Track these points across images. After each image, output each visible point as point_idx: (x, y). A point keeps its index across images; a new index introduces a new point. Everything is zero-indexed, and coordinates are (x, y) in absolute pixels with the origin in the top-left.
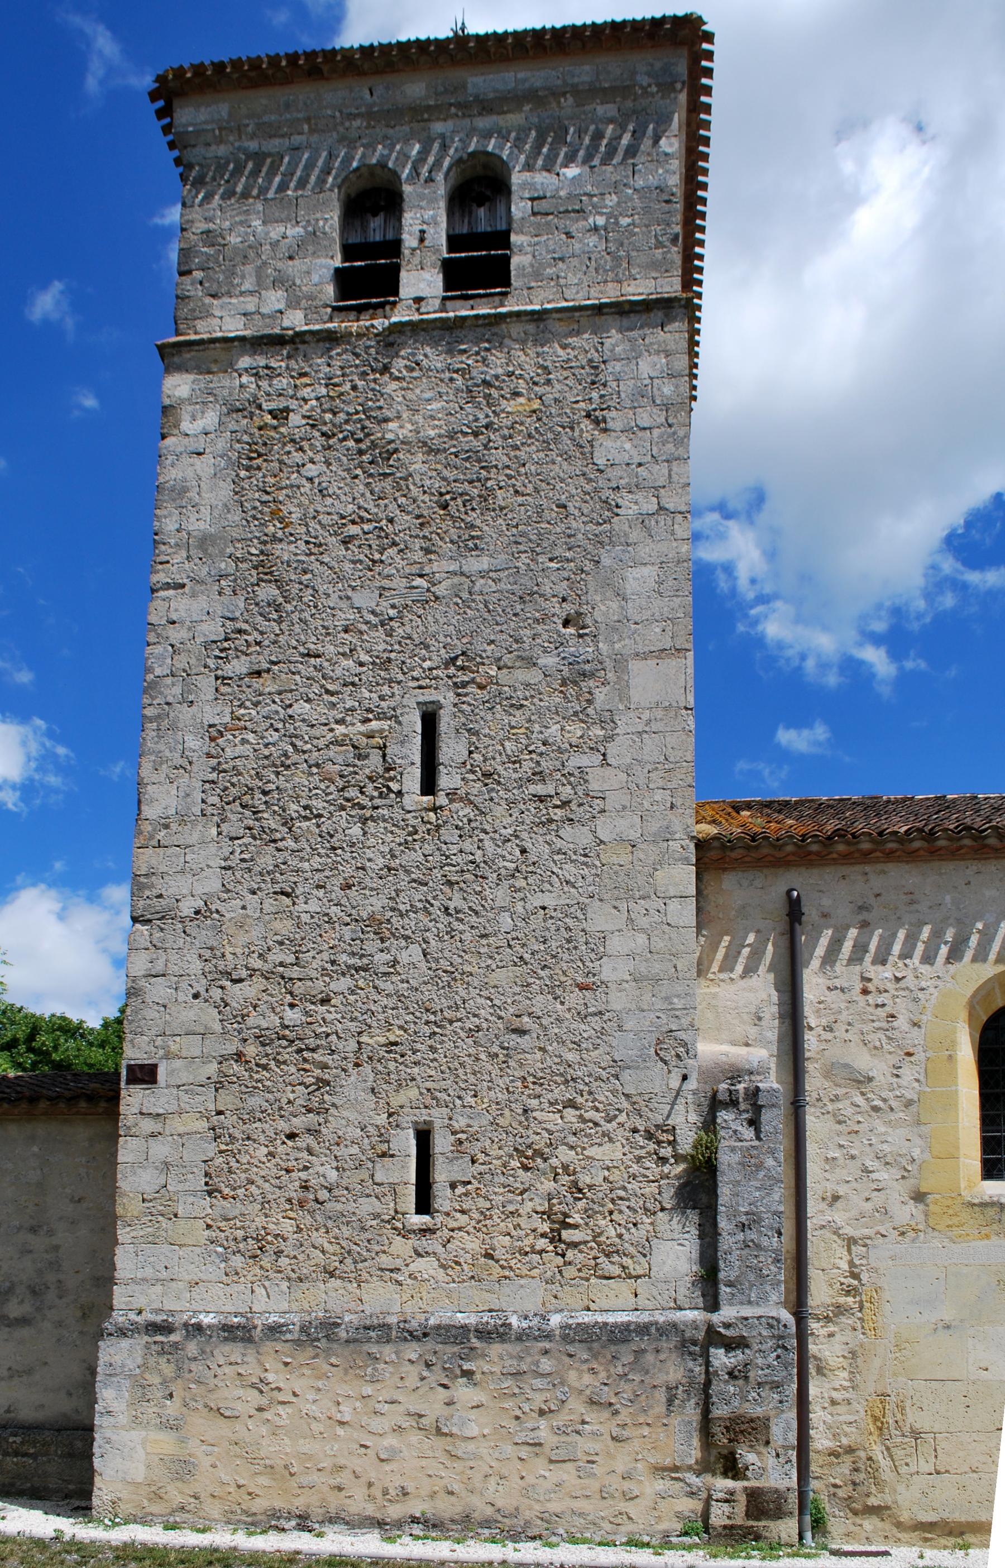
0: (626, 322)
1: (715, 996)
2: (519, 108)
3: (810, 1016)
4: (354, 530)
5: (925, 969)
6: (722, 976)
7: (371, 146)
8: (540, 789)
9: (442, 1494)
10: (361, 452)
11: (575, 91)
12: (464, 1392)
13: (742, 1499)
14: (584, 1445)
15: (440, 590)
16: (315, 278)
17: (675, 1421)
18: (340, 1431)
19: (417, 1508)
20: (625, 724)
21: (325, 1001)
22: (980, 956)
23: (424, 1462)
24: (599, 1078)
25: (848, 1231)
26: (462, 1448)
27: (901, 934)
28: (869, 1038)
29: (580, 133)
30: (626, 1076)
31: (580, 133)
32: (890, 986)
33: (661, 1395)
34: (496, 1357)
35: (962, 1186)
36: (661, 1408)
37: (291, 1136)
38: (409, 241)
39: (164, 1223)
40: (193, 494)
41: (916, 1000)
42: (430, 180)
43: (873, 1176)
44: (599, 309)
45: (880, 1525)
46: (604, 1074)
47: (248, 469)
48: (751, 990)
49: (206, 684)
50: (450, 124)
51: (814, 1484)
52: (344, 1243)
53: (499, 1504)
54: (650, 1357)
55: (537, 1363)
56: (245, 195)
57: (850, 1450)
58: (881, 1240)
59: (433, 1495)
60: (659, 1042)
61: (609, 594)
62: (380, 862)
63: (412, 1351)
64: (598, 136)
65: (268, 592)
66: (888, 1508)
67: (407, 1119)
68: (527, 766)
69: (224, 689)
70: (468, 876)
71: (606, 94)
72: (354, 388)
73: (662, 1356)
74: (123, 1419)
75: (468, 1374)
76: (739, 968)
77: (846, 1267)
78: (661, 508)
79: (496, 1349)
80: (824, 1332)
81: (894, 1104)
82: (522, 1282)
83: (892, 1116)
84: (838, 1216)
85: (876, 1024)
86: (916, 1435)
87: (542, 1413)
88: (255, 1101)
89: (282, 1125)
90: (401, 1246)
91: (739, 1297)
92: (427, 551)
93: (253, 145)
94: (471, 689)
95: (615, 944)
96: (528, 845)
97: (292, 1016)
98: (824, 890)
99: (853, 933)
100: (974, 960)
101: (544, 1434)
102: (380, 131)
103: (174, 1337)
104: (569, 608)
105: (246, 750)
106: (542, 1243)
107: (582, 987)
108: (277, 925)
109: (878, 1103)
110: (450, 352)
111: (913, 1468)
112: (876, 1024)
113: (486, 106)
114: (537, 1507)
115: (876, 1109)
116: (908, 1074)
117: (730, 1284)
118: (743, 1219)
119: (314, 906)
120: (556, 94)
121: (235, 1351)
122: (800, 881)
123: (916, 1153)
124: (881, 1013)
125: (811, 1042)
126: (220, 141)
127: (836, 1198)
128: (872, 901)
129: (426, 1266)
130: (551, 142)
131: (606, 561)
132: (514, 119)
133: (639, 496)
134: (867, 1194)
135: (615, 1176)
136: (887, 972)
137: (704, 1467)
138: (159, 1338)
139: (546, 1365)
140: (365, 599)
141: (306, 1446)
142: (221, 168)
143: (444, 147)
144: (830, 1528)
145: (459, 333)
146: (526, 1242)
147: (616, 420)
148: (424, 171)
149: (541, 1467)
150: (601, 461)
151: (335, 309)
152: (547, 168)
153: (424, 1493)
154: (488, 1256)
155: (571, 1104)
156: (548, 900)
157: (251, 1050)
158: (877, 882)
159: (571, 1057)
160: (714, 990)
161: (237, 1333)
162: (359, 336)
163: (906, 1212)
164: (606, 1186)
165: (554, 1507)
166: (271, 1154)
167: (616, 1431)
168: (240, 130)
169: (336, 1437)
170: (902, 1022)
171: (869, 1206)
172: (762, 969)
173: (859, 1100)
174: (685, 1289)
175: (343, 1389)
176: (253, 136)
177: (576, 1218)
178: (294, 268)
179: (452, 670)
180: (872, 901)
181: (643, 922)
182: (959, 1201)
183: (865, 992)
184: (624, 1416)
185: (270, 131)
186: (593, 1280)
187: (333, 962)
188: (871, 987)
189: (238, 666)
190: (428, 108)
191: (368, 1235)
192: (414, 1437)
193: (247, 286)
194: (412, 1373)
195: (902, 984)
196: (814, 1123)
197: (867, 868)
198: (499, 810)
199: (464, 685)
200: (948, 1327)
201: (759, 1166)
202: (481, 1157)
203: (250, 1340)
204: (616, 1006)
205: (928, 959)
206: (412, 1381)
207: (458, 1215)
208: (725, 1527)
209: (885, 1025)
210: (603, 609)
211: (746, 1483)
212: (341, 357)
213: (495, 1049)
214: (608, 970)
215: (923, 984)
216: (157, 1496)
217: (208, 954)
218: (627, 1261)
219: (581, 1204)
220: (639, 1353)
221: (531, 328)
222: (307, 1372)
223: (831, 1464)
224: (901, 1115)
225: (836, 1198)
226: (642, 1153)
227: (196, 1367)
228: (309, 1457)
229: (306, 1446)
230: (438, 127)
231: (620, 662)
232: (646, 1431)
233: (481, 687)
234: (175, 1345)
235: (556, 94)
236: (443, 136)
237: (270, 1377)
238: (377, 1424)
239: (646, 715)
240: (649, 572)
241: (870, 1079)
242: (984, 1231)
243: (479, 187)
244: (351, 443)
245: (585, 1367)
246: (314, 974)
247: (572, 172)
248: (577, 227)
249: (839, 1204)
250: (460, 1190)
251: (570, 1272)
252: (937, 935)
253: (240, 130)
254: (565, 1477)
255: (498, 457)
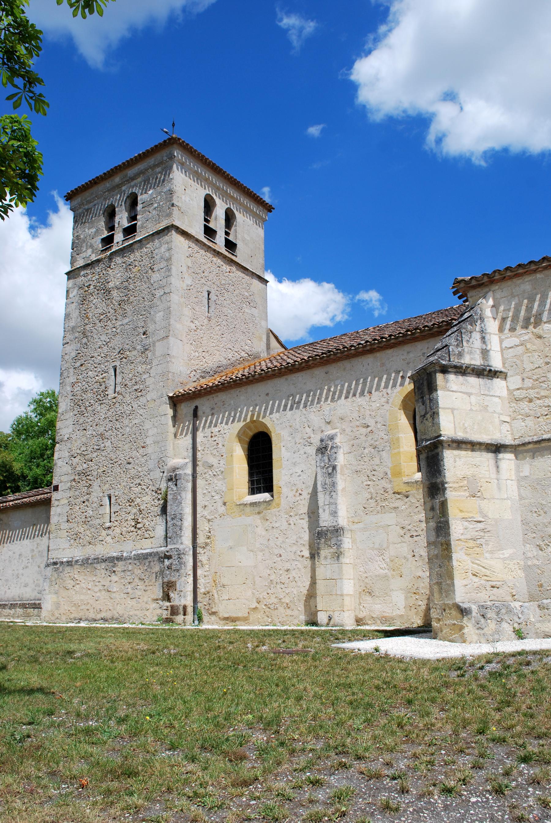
0: (159, 236)
1: (178, 443)
2: (140, 176)
3: (199, 447)
4: (102, 317)
5: (226, 427)
6: (181, 437)
7: (109, 199)
8: (136, 387)
9: (108, 610)
10: (104, 293)
11: (150, 167)
12: (114, 578)
13: (170, 608)
14: (138, 593)
15: (118, 331)
16: (97, 243)
17: (157, 584)
18: (89, 592)
19: (103, 615)
20: (155, 362)
21: (91, 461)
22: (239, 421)
23: (105, 601)
24: (145, 476)
25: (208, 517)
26: (113, 595)
27: (221, 416)
28: (212, 452)
29: (153, 179)
30: (151, 473)
31: (153, 179)
32: (217, 434)
33: (154, 575)
34: (121, 565)
35: (235, 499)
36: (154, 580)
37: (84, 502)
38: (116, 225)
39: (59, 532)
40: (71, 315)
41: (223, 437)
42: (121, 205)
43: (214, 498)
44: (153, 235)
45: (215, 618)
46: (146, 474)
47: (82, 304)
48: (186, 440)
49: (72, 370)
50: (126, 187)
51: (199, 605)
52: (93, 533)
53: (120, 613)
54: (152, 563)
55: (128, 567)
56: (85, 223)
57: (208, 593)
58: (216, 519)
59: (106, 610)
60: (159, 462)
61: (153, 322)
62: (103, 416)
63: (103, 565)
64: (157, 178)
65: (85, 340)
66: (217, 612)
67: (106, 494)
68: (133, 381)
69: (75, 371)
70: (121, 417)
71: (157, 165)
72: (103, 274)
73: (155, 563)
74: (47, 591)
75: (114, 572)
76: (184, 434)
77: (208, 529)
78: (165, 293)
79: (120, 563)
80: (203, 552)
81: (218, 473)
82: (128, 541)
83: (219, 477)
84: (206, 513)
85: (214, 447)
86: (224, 586)
87: (129, 583)
88: (77, 493)
89: (82, 499)
90: (104, 533)
91: (172, 542)
92: (116, 320)
93: (86, 207)
94: (124, 360)
95: (150, 433)
96: (133, 405)
97: (85, 466)
98: (204, 405)
99: (210, 417)
100: (238, 422)
101: (129, 590)
102: (112, 193)
103: (58, 566)
104: (144, 329)
105: (79, 388)
106: (133, 529)
107: (143, 447)
108: (83, 439)
109: (215, 473)
110: (123, 257)
111: (223, 598)
112: (214, 447)
113: (133, 179)
114: (127, 614)
115: (214, 475)
116: (222, 462)
117: (170, 538)
118: (173, 516)
119: (90, 433)
120: (146, 170)
121: (68, 569)
122: (197, 402)
123: (224, 489)
124: (215, 443)
125: (199, 455)
126: (80, 208)
127: (205, 506)
128: (215, 406)
129: (109, 539)
130: (147, 184)
131: (152, 313)
132: (139, 180)
133: (160, 291)
134: (212, 504)
135: (149, 505)
136: (217, 429)
137: (163, 599)
138: (55, 566)
139: (130, 567)
140: (103, 338)
141: (82, 597)
142: (80, 216)
143: (124, 194)
144: (204, 620)
145: (124, 251)
146: (129, 529)
147: (156, 268)
148: (120, 203)
149: (129, 601)
150: (152, 282)
151: (102, 251)
152: (145, 193)
153: (105, 610)
154: (121, 534)
155: (140, 484)
156: (136, 421)
157: (77, 478)
158: (216, 399)
159: (140, 469)
160: (179, 442)
161: (69, 563)
162: (105, 258)
163: (222, 509)
164: (146, 509)
165: (131, 613)
166: (80, 508)
167: (145, 588)
168: (83, 204)
169: (88, 594)
170: (220, 446)
171: (213, 508)
172: (189, 433)
173: (211, 473)
174: (162, 541)
175: (90, 579)
176: (86, 204)
177: (140, 520)
178: (93, 241)
179: (120, 355)
180: (215, 406)
181: (156, 424)
182: (234, 504)
183: (212, 437)
184: (146, 583)
185: (89, 202)
186: (143, 539)
187: (93, 448)
188: (213, 435)
189: (78, 364)
190: (120, 184)
191: (97, 531)
192: (103, 592)
193: (84, 250)
194: (104, 571)
195: (220, 433)
196: (200, 482)
197: (214, 395)
198: (127, 396)
199: (122, 359)
200: (231, 548)
201: (177, 499)
202: (121, 504)
203: (71, 565)
204: (150, 452)
205: (278, 411)
206: (103, 575)
207: (115, 522)
208: (166, 618)
209: (216, 447)
210: (151, 328)
211: (171, 604)
212: (101, 265)
213: (124, 469)
214: (149, 441)
215: (225, 432)
216: (53, 615)
217: (69, 450)
218: (150, 532)
219: (141, 516)
220: (150, 562)
221: (139, 245)
222: (83, 574)
223: (204, 597)
224: (221, 476)
225: (205, 506)
226: (154, 498)
227: (61, 574)
228: (82, 600)
229: (82, 597)
230: (123, 188)
231: (154, 343)
232: (151, 587)
233: (126, 358)
234: (58, 568)
235: (146, 170)
236: (124, 191)
237: (76, 576)
238: (96, 589)
239: (159, 359)
240: (161, 314)
241: (213, 466)
242: (240, 513)
243: (133, 202)
244: (102, 291)
245: (138, 567)
246: (89, 453)
247: (150, 192)
248: (151, 209)
249: (206, 508)
250: (116, 514)
251: (138, 537)
252: (230, 414)
253: (83, 204)
254: (134, 603)
255: (131, 286)
